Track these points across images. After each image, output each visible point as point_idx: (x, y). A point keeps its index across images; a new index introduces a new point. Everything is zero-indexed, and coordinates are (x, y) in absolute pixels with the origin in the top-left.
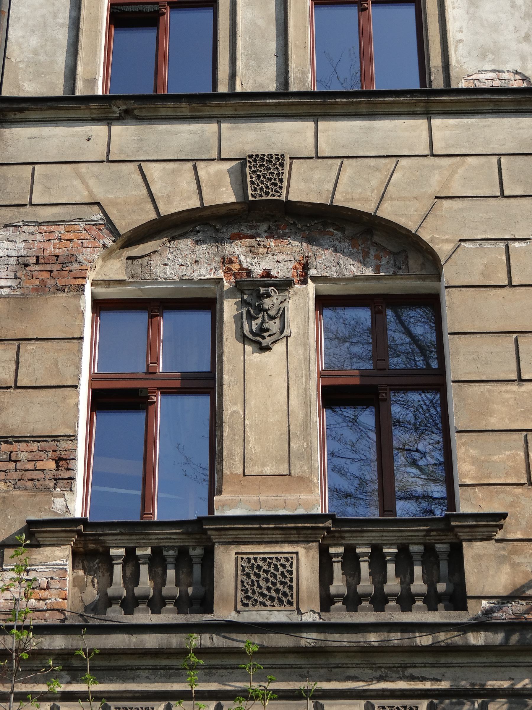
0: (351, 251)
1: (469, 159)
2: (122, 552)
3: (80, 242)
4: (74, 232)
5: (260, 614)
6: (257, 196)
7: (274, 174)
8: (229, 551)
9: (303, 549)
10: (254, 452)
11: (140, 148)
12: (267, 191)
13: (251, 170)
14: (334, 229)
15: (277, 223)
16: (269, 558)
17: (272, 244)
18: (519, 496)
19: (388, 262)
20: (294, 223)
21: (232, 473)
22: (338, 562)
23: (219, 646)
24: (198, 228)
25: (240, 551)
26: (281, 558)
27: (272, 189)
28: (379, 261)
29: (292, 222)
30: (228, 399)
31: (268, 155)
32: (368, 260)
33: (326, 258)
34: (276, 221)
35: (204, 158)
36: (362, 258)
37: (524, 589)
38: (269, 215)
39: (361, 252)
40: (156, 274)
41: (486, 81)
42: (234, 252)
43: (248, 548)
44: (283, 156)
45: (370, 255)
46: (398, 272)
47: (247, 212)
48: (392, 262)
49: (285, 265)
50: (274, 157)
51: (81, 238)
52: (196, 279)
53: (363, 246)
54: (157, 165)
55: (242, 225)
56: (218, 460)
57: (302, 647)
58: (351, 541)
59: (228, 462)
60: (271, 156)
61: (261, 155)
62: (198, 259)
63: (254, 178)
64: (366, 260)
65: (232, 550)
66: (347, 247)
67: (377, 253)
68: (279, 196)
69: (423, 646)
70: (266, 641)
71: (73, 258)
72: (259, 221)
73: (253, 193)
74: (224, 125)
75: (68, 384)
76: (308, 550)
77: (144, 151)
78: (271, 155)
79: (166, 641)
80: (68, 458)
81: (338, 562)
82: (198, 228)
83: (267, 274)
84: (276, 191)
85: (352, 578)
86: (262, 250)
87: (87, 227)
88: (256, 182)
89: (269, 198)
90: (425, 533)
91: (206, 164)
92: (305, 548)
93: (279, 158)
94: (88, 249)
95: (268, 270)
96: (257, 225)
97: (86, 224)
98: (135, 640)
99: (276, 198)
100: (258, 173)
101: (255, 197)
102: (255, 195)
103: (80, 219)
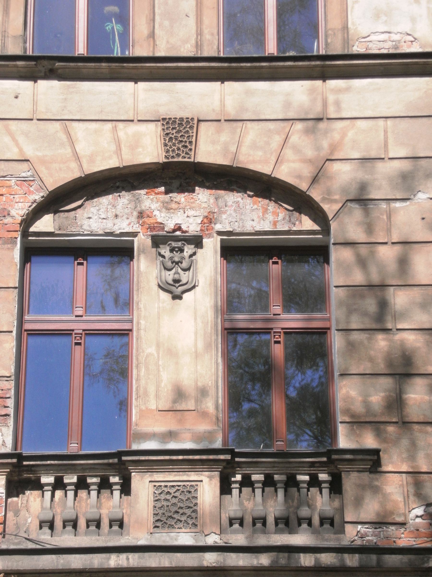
0: (252, 207)
1: (359, 122)
2: (51, 480)
3: (12, 196)
4: (7, 187)
5: (169, 536)
6: (170, 158)
7: (185, 136)
8: (144, 480)
9: (206, 478)
10: (166, 390)
11: (65, 107)
12: (179, 153)
13: (165, 133)
14: (237, 187)
15: (188, 180)
16: (177, 486)
17: (183, 200)
18: (391, 433)
19: (284, 218)
20: (203, 181)
21: (147, 408)
22: (236, 488)
23: (134, 565)
24: (118, 184)
25: (153, 480)
26: (188, 485)
27: (183, 151)
28: (276, 217)
29: (200, 180)
30: (144, 342)
31: (180, 118)
32: (267, 216)
33: (231, 214)
34: (187, 179)
35: (122, 118)
36: (261, 214)
37: (394, 516)
38: (181, 173)
39: (261, 208)
40: (81, 226)
41: (378, 43)
42: (150, 208)
43: (160, 477)
44: (192, 119)
45: (269, 211)
46: (292, 227)
47: (161, 171)
48: (287, 218)
49: (194, 220)
50: (185, 120)
51: (13, 193)
52: (118, 232)
53: (262, 203)
54: (81, 124)
55: (156, 182)
56: (135, 397)
57: (205, 567)
58: (247, 471)
59: (144, 399)
60: (181, 119)
61: (174, 118)
62: (118, 213)
63: (167, 141)
64: (265, 216)
65: (146, 479)
66: (249, 204)
67: (274, 210)
68: (189, 158)
69: (306, 567)
70: (174, 562)
71: (6, 213)
72: (171, 178)
73: (166, 155)
74: (347, 519)
75: (5, 330)
76: (210, 478)
77: (68, 111)
78: (182, 118)
79: (89, 562)
80: (4, 396)
81: (236, 488)
82: (118, 184)
83: (179, 228)
84: (187, 153)
85: (248, 502)
86: (174, 206)
87: (18, 182)
88: (169, 145)
89: (180, 159)
90: (310, 464)
91: (125, 125)
92: (208, 477)
93: (189, 121)
94: (20, 204)
95: (179, 224)
96: (170, 182)
97: (18, 180)
98: (62, 561)
99: (186, 160)
100: (171, 136)
101: (168, 158)
102: (168, 157)
103: (12, 175)
